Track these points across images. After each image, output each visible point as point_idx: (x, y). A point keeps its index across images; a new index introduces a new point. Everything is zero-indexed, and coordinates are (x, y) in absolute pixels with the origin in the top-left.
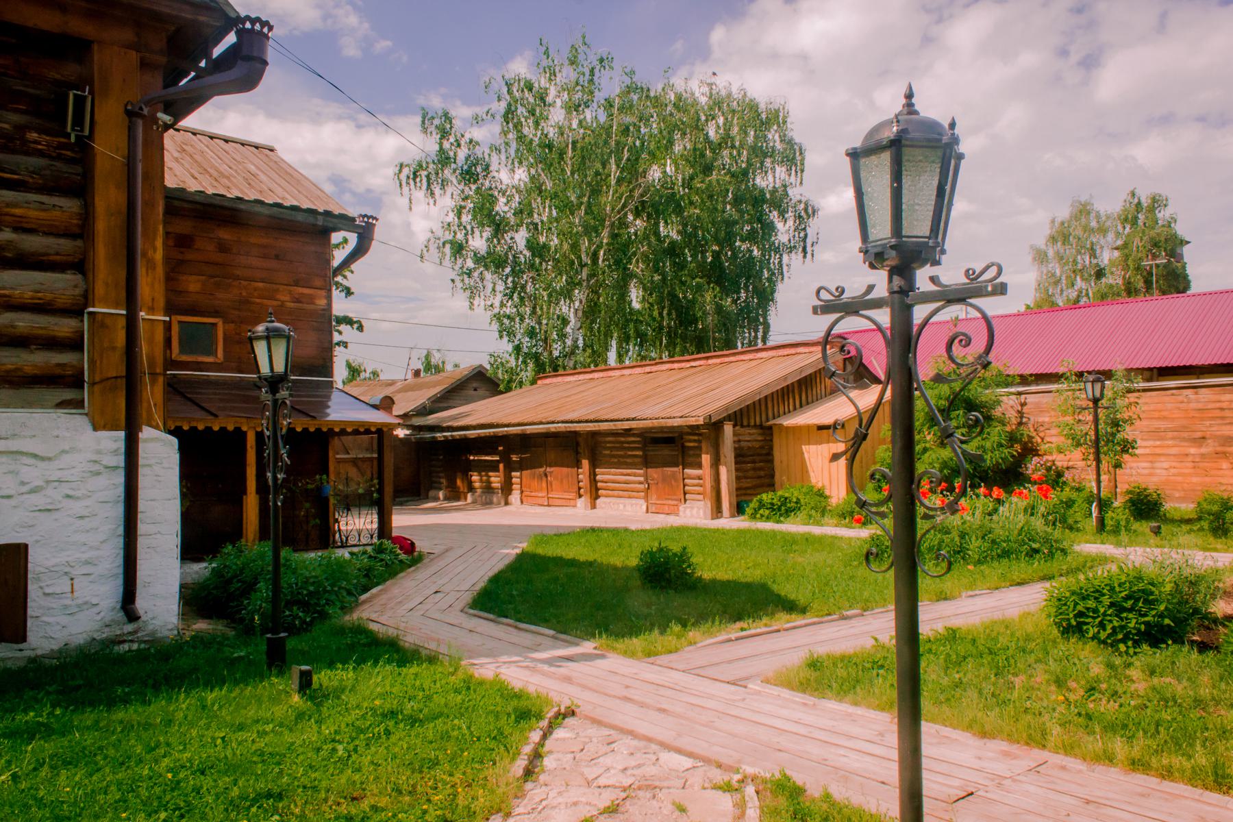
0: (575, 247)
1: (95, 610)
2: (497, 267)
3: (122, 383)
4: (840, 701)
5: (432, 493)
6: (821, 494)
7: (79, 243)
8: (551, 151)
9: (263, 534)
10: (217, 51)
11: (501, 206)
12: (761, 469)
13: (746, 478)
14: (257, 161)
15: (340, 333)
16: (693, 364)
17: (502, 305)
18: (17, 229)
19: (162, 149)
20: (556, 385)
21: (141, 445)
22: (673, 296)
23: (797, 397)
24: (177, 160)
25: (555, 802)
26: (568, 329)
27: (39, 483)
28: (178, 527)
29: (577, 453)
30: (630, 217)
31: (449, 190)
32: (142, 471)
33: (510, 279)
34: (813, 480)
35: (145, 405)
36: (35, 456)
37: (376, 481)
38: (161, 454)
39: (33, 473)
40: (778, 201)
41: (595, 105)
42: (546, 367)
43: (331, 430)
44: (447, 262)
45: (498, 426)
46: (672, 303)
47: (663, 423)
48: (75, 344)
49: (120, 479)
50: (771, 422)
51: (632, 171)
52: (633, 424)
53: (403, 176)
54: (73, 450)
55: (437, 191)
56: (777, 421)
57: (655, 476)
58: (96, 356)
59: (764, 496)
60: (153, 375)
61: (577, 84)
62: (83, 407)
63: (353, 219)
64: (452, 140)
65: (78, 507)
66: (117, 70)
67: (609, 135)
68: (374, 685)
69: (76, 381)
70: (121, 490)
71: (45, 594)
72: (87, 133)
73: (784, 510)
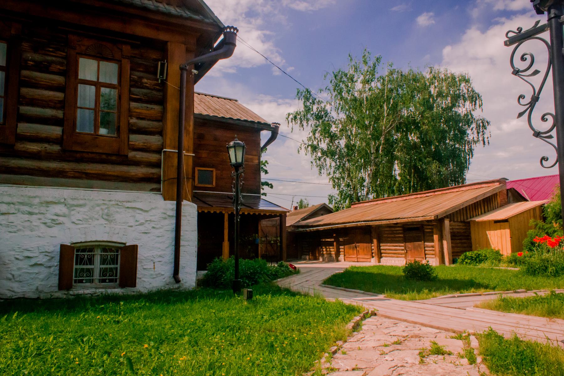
0: (368, 145)
1: (163, 277)
2: (332, 156)
3: (176, 180)
4: (519, 313)
5: (303, 257)
6: (497, 252)
7: (161, 123)
8: (356, 102)
9: (231, 253)
10: (215, 45)
11: (333, 129)
12: (465, 243)
13: (458, 247)
14: (230, 104)
15: (263, 189)
16: (427, 195)
17: (334, 172)
18: (138, 118)
19: (193, 100)
20: (360, 207)
21: (182, 207)
22: (415, 167)
23: (483, 208)
24: (199, 104)
25: (368, 339)
26: (365, 184)
27: (143, 221)
28: (196, 243)
29: (371, 236)
30: (393, 132)
31: (310, 123)
32: (183, 218)
33: (338, 161)
34: (493, 247)
35: (184, 191)
36: (142, 210)
37: (279, 239)
38: (190, 210)
39: (141, 217)
40: (468, 120)
41: (376, 80)
42: (355, 200)
43: (259, 214)
44: (309, 154)
45: (333, 224)
46: (415, 170)
47: (413, 219)
48: (157, 165)
49: (174, 221)
50: (469, 220)
51: (394, 109)
52: (399, 221)
53: (290, 119)
54: (155, 208)
55: (305, 123)
56: (473, 219)
57: (410, 246)
58: (166, 170)
59: (468, 253)
60: (188, 178)
61: (368, 71)
62: (160, 191)
63: (269, 125)
64: (311, 101)
65: (157, 232)
66: (178, 57)
67: (383, 94)
68: (281, 301)
69: (157, 180)
70: (174, 226)
71: (144, 269)
72: (165, 78)
73: (478, 259)
